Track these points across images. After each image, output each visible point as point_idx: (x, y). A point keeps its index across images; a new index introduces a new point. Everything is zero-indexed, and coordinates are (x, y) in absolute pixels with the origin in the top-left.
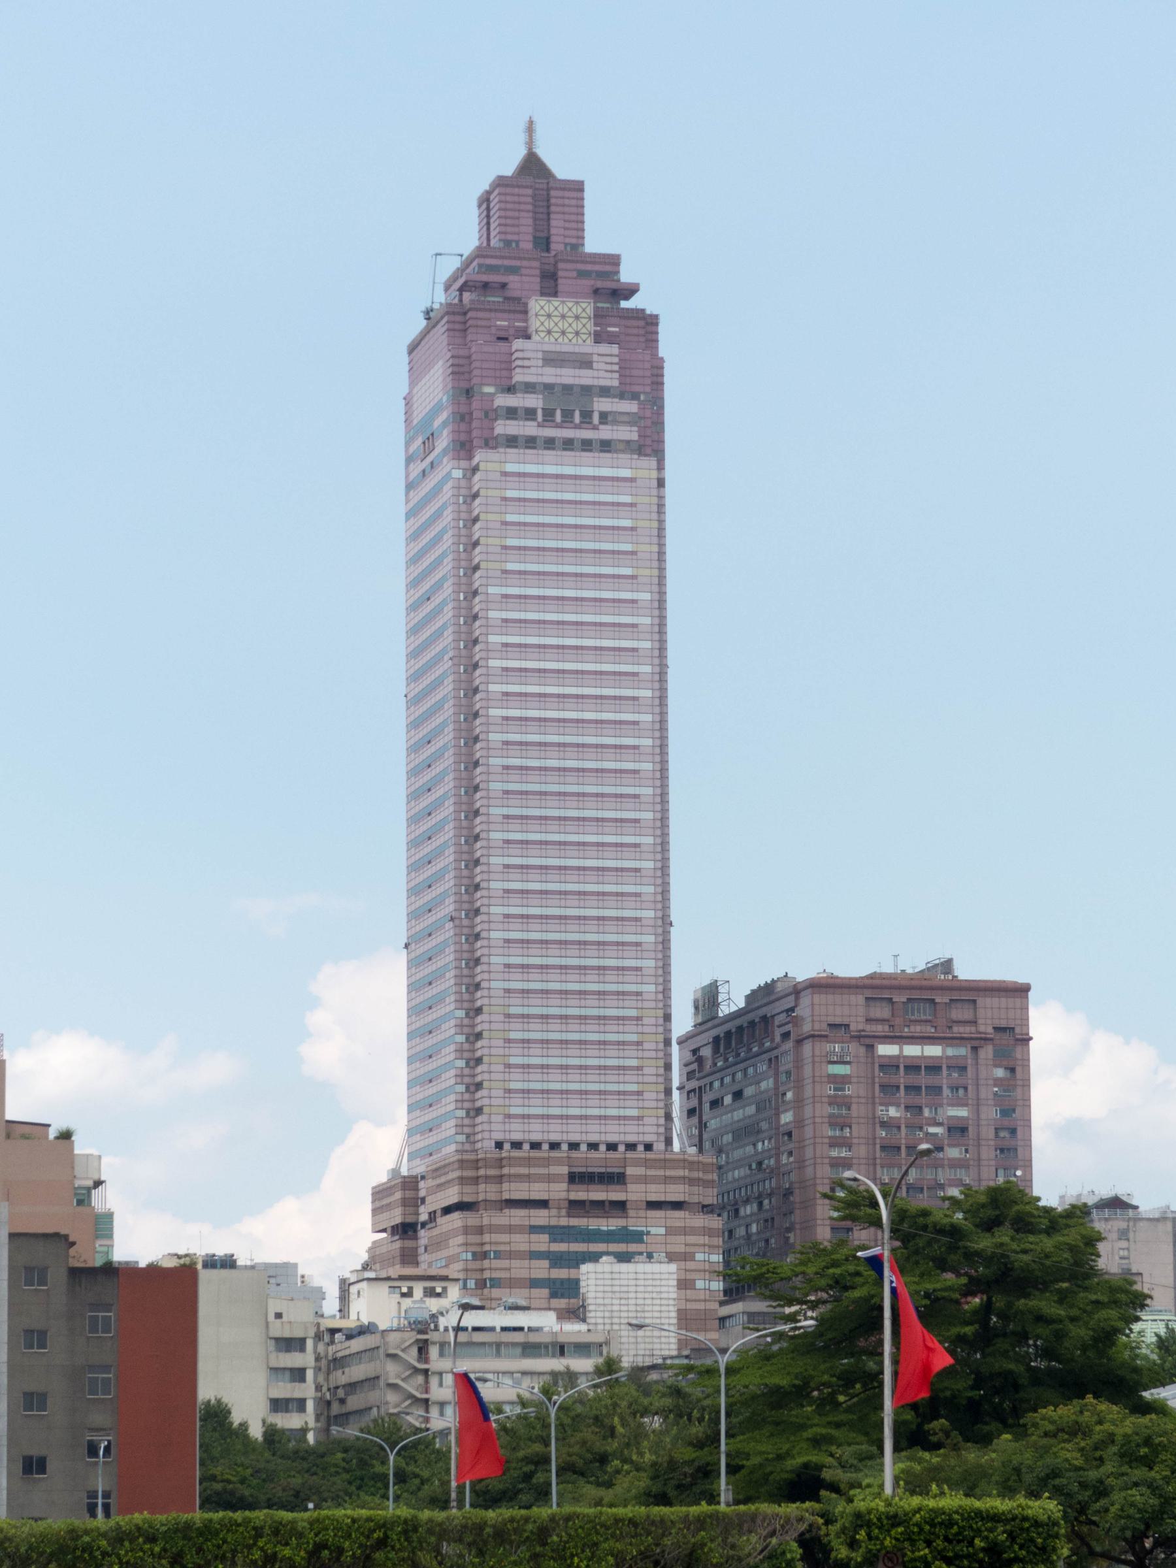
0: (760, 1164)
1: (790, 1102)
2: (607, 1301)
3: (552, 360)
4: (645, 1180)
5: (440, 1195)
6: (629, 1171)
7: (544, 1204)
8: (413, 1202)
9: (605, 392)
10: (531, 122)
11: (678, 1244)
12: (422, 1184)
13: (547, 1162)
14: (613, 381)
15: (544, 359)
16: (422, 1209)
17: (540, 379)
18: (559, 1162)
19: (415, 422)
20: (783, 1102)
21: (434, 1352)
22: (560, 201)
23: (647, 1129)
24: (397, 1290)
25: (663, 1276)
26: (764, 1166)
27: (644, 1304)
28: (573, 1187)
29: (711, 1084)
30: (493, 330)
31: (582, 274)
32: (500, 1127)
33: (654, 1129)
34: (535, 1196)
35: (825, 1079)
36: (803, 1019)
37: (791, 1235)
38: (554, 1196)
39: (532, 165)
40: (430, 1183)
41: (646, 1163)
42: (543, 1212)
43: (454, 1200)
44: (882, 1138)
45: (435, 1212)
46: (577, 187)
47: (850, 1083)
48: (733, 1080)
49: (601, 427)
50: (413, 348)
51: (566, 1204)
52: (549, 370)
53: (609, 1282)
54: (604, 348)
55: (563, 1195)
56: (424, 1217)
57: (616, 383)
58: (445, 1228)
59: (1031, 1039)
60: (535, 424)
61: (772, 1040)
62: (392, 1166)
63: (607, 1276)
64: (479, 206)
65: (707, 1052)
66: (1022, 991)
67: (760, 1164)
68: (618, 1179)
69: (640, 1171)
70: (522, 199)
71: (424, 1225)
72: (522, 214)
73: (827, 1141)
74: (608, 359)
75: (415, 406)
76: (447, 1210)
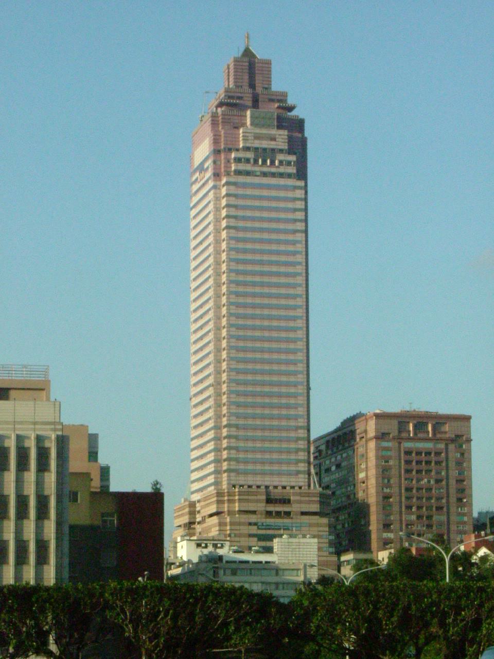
4: (300, 502)
5: (207, 509)
6: (292, 498)
7: (254, 512)
8: (193, 513)
9: (281, 151)
12: (198, 505)
13: (255, 494)
14: (285, 147)
15: (254, 137)
16: (197, 516)
17: (253, 145)
21: (221, 572)
23: (300, 480)
27: (299, 556)
28: (268, 505)
38: (259, 509)
39: (247, 53)
40: (203, 503)
41: (300, 494)
42: (254, 516)
43: (214, 510)
45: (205, 517)
46: (268, 63)
51: (264, 512)
52: (256, 141)
54: (281, 132)
56: (198, 520)
57: (286, 148)
58: (210, 524)
59: (471, 440)
63: (287, 544)
65: (323, 447)
66: (467, 419)
68: (287, 501)
69: (298, 498)
71: (199, 523)
76: (211, 516)
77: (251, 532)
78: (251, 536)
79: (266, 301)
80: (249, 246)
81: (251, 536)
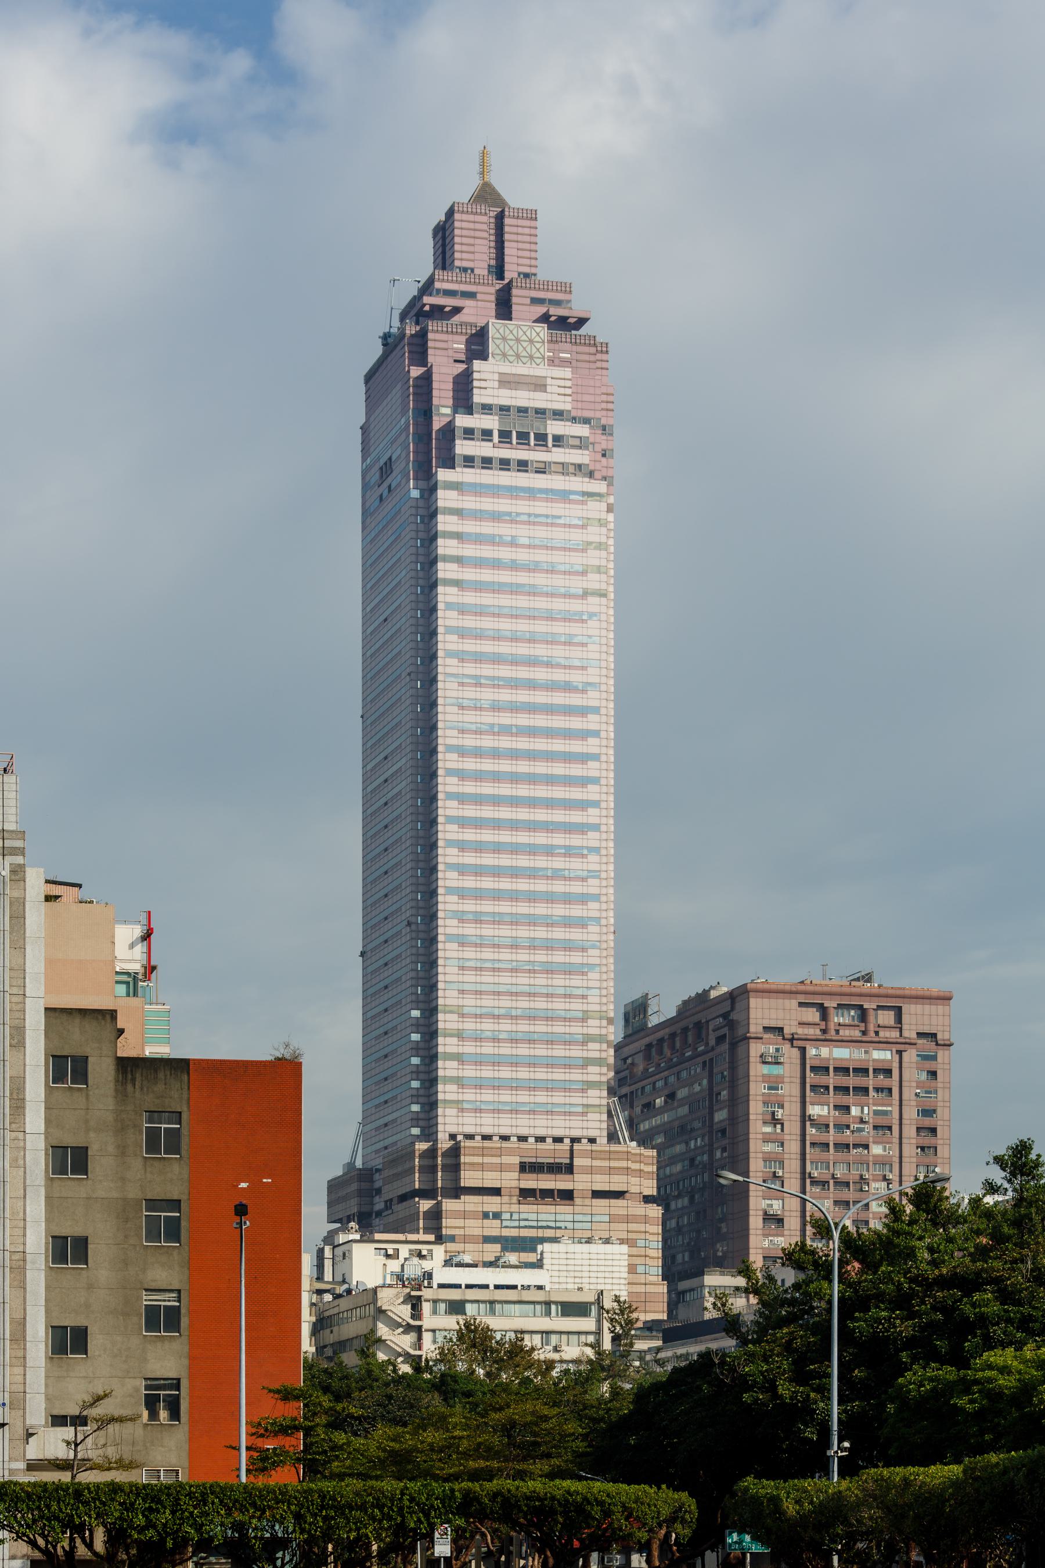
0: (692, 1160)
1: (724, 1101)
2: (562, 1280)
3: (507, 382)
4: (591, 1170)
7: (496, 1192)
9: (558, 415)
10: (483, 154)
11: (620, 1230)
12: (377, 1176)
15: (499, 381)
18: (511, 1152)
19: (399, 386)
20: (717, 1101)
21: (426, 1307)
22: (514, 230)
23: (591, 1124)
24: (383, 1252)
25: (615, 1257)
26: (697, 1162)
29: (643, 1088)
30: (450, 353)
31: (535, 301)
32: (454, 1120)
33: (597, 1125)
34: (488, 1184)
35: (761, 1079)
36: (738, 1022)
37: (723, 1225)
38: (505, 1184)
41: (593, 1156)
42: (496, 1199)
44: (812, 1135)
45: (391, 1200)
47: (783, 1082)
48: (666, 1084)
49: (554, 449)
50: (369, 378)
51: (517, 1192)
53: (564, 1262)
55: (515, 1184)
60: (490, 444)
61: (707, 1044)
62: (347, 1160)
64: (434, 237)
67: (692, 1160)
70: (478, 226)
71: (379, 1214)
72: (478, 241)
73: (761, 1136)
74: (562, 383)
75: (372, 435)
77: (488, 1232)
78: (487, 1240)
79: (523, 838)
80: (487, 836)
81: (487, 1240)
